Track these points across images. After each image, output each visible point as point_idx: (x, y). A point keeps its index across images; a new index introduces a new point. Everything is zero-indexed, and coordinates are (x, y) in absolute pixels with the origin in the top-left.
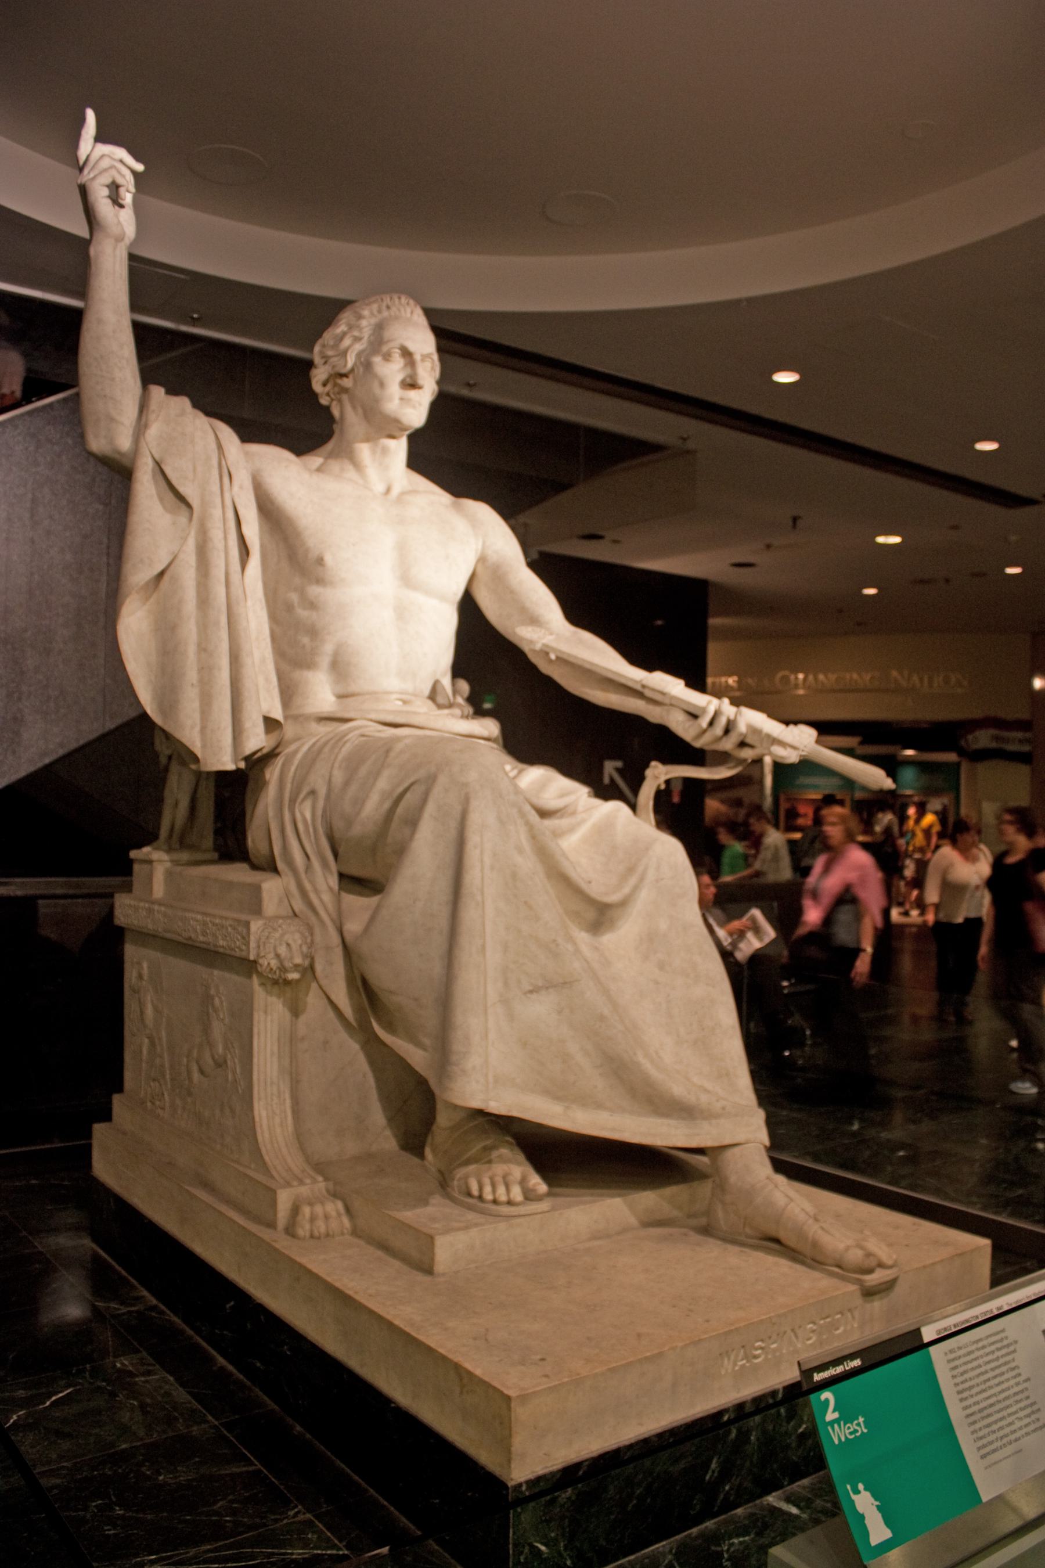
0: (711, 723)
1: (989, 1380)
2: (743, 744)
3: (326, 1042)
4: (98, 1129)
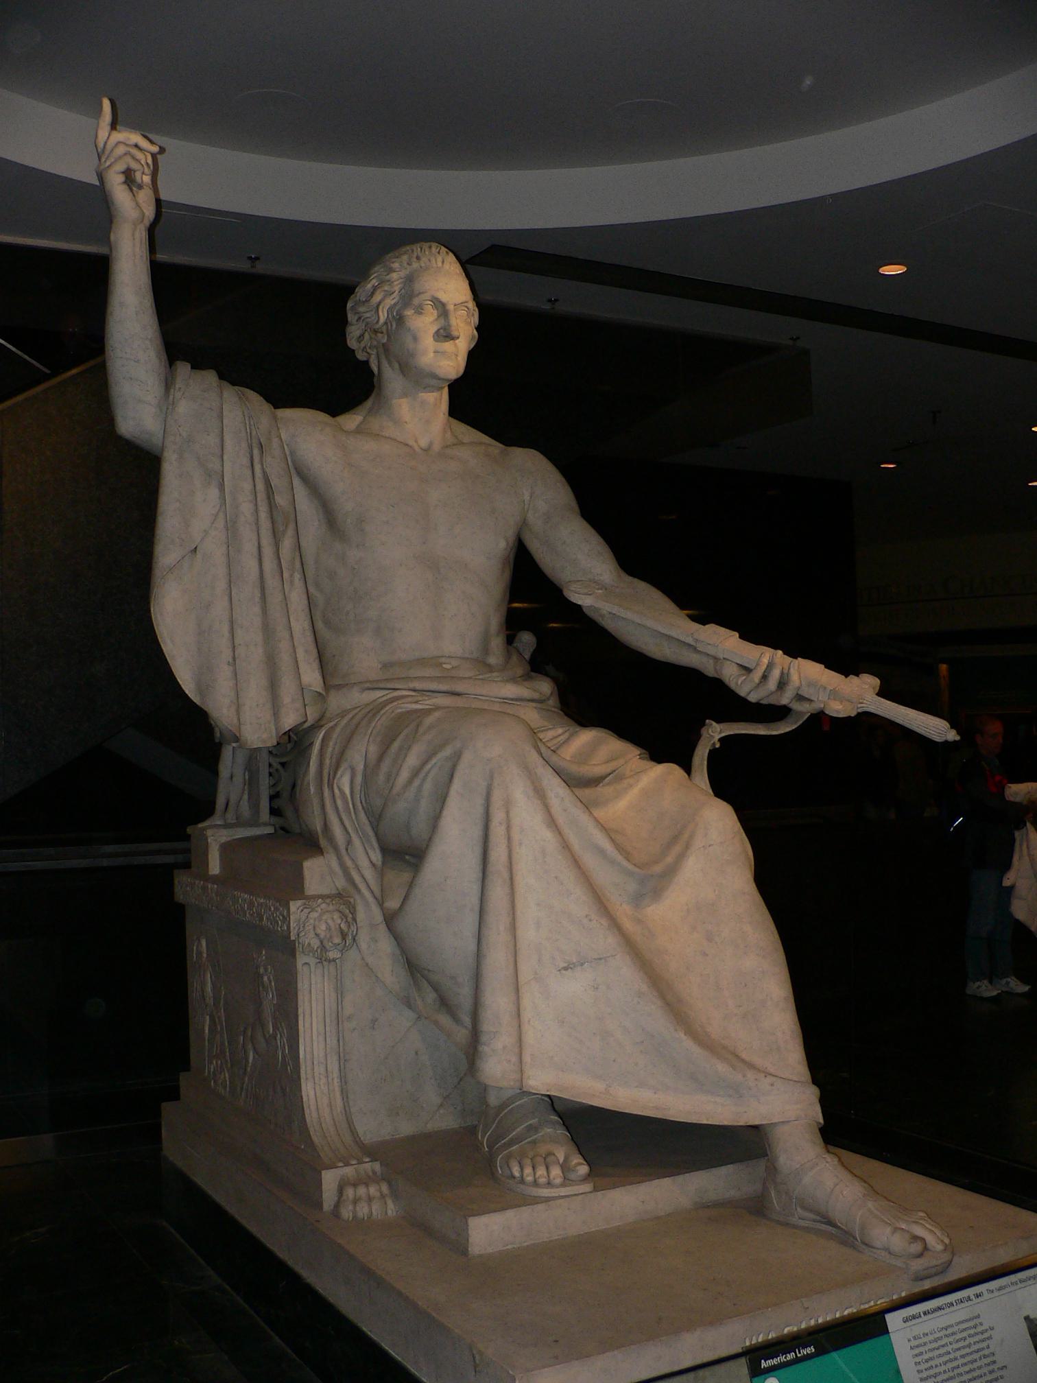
0: (765, 677)
1: (958, 1367)
3: (374, 1021)
4: (167, 1107)
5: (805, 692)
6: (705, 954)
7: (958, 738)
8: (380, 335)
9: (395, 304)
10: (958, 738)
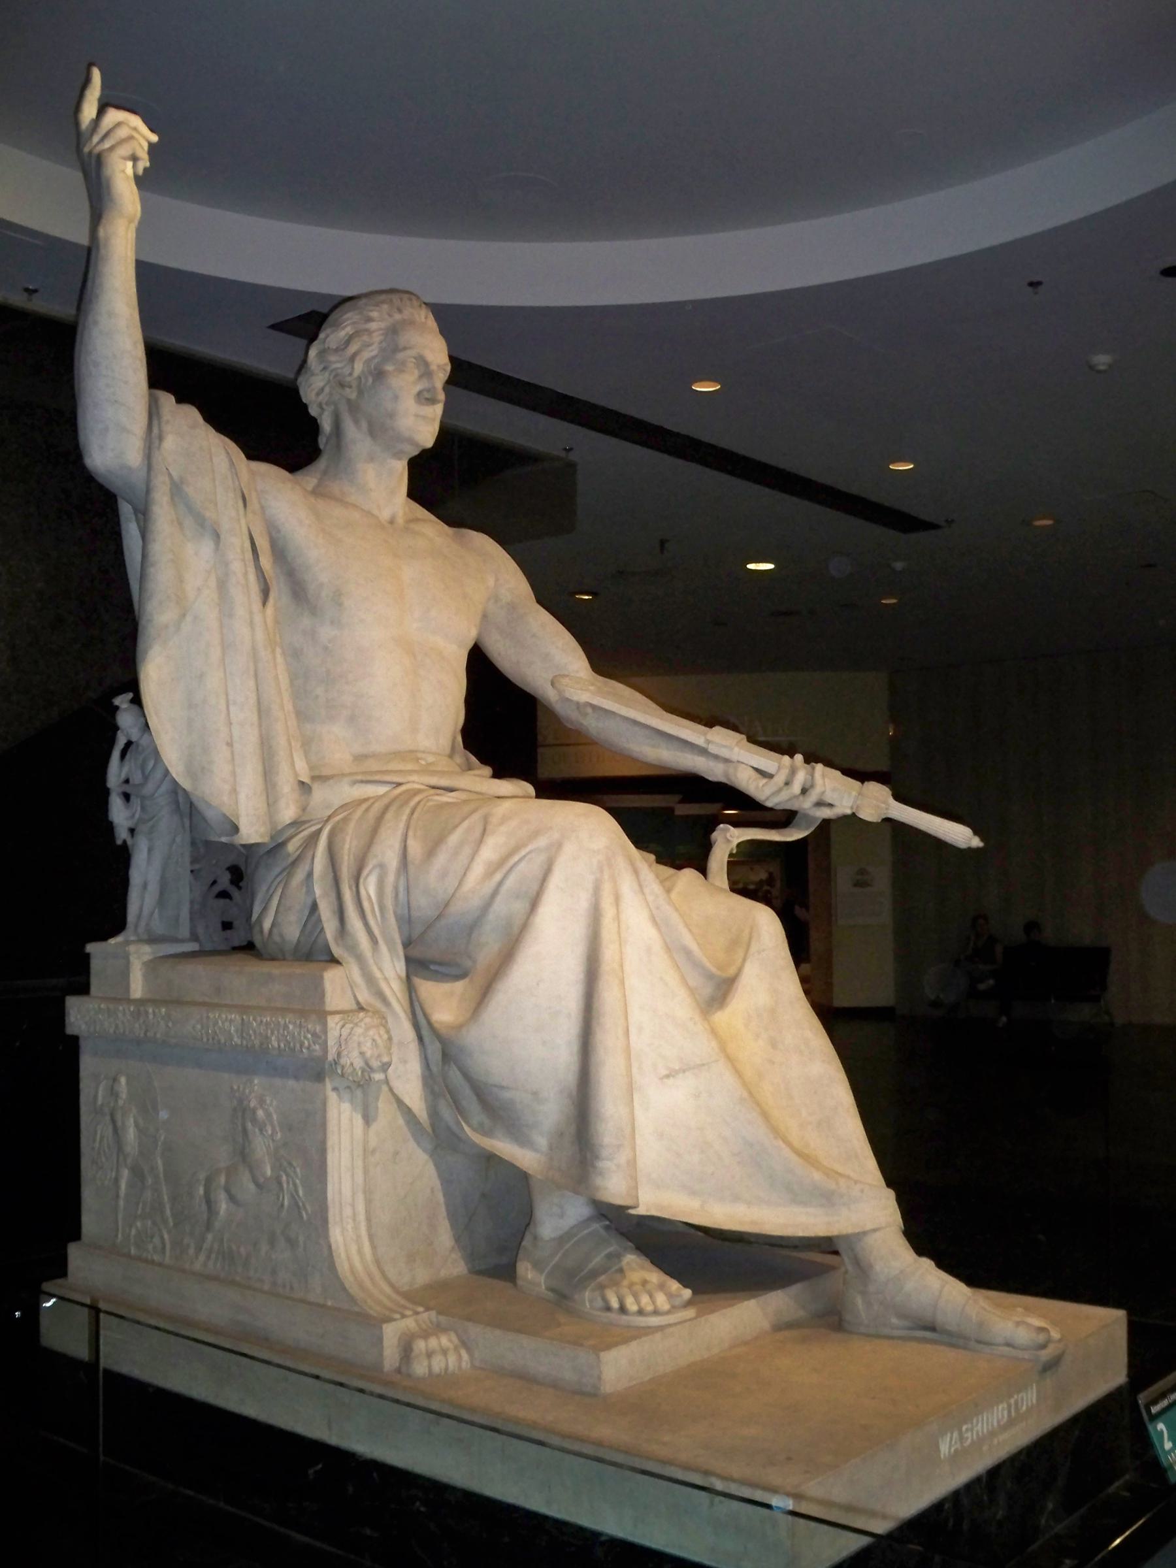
2: (820, 804)
3: (397, 1153)
5: (828, 798)
6: (772, 1062)
7: (981, 844)
8: (348, 390)
9: (374, 357)
10: (981, 844)
